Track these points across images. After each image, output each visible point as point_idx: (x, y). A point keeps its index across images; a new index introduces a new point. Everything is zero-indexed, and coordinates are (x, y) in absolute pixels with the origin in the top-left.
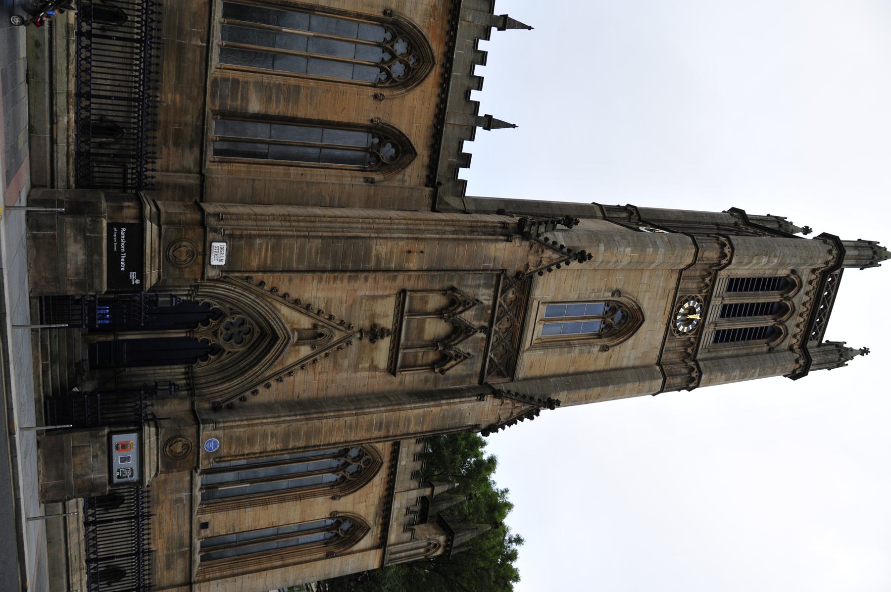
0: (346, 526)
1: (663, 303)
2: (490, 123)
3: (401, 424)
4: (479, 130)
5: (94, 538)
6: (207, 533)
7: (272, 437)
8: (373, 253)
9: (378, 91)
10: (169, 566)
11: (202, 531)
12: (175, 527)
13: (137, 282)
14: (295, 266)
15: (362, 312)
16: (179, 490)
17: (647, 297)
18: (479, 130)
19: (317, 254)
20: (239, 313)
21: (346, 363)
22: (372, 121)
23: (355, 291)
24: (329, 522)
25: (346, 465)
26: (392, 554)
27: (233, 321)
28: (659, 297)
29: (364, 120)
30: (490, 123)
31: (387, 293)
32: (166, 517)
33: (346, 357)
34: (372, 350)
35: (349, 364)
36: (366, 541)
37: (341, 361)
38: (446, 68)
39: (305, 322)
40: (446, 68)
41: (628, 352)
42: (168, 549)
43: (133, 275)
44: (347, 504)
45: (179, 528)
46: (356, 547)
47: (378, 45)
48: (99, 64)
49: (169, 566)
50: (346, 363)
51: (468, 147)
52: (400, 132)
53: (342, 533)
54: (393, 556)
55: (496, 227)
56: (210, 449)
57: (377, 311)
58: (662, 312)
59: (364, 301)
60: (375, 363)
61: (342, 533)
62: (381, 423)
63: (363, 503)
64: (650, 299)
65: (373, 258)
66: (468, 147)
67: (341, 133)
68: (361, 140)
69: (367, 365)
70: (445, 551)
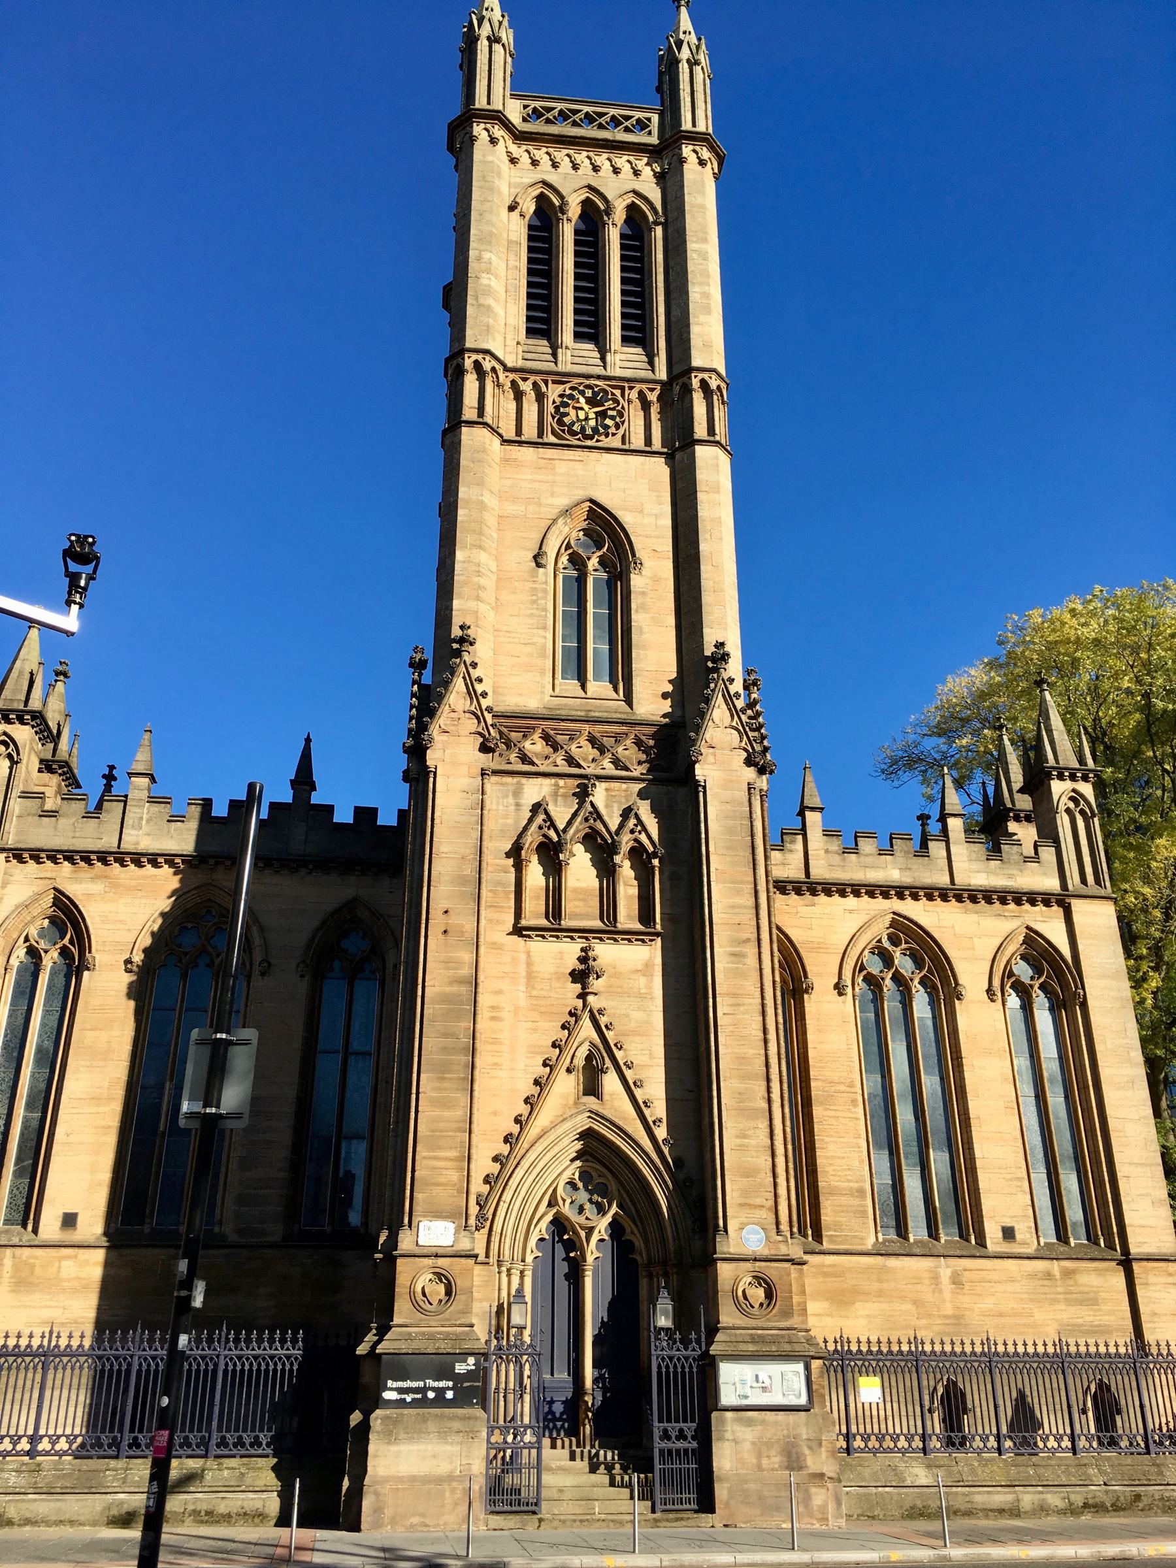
0: (1023, 971)
1: (562, 467)
2: (304, 780)
3: (737, 919)
4: (316, 798)
5: (881, 1438)
6: (1024, 1231)
7: (745, 1137)
8: (448, 989)
9: (256, 970)
10: (1090, 1300)
11: (1018, 1236)
12: (1009, 1287)
13: (471, 1360)
14: (460, 1113)
15: (553, 994)
16: (936, 1279)
17: (550, 501)
18: (316, 798)
19: (443, 1079)
20: (555, 1190)
21: (637, 1015)
22: (302, 976)
23: (517, 1009)
24: (1014, 1001)
25: (898, 978)
26: (1084, 881)
27: (568, 1201)
28: (550, 478)
29: (302, 988)
30: (304, 780)
31: (523, 957)
32: (988, 1303)
33: (627, 1016)
34: (617, 975)
35: (639, 1009)
36: (1053, 929)
37: (633, 1025)
38: (217, 863)
39: (566, 1086)
40: (217, 863)
41: (647, 520)
42: (1056, 1301)
43: (460, 1368)
44: (972, 975)
45: (1012, 1280)
46: (1066, 951)
47: (184, 976)
48: (70, 1421)
49: (1090, 1300)
50: (637, 1015)
51: (344, 815)
52: (319, 928)
53: (1049, 975)
54: (1090, 878)
55: (416, 790)
56: (760, 1241)
57: (552, 969)
58: (578, 465)
59: (534, 993)
60: (640, 968)
61: (1049, 975)
62: (733, 954)
63: (974, 941)
64: (552, 495)
65: (454, 989)
66: (344, 815)
67: (324, 1023)
68: (334, 989)
69: (643, 980)
70: (1085, 779)
